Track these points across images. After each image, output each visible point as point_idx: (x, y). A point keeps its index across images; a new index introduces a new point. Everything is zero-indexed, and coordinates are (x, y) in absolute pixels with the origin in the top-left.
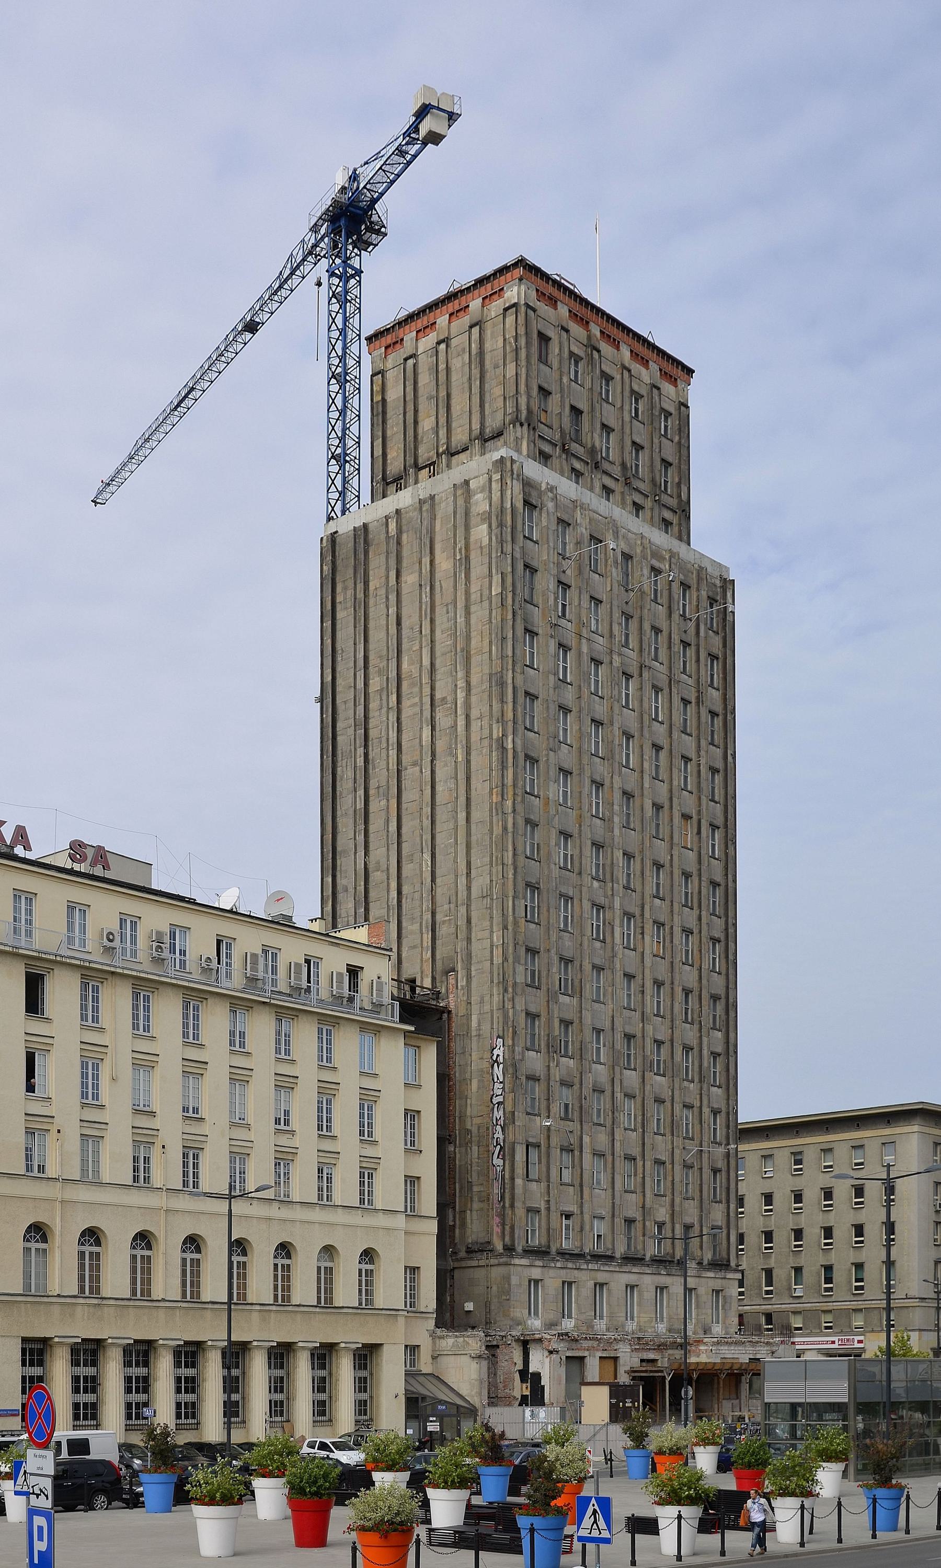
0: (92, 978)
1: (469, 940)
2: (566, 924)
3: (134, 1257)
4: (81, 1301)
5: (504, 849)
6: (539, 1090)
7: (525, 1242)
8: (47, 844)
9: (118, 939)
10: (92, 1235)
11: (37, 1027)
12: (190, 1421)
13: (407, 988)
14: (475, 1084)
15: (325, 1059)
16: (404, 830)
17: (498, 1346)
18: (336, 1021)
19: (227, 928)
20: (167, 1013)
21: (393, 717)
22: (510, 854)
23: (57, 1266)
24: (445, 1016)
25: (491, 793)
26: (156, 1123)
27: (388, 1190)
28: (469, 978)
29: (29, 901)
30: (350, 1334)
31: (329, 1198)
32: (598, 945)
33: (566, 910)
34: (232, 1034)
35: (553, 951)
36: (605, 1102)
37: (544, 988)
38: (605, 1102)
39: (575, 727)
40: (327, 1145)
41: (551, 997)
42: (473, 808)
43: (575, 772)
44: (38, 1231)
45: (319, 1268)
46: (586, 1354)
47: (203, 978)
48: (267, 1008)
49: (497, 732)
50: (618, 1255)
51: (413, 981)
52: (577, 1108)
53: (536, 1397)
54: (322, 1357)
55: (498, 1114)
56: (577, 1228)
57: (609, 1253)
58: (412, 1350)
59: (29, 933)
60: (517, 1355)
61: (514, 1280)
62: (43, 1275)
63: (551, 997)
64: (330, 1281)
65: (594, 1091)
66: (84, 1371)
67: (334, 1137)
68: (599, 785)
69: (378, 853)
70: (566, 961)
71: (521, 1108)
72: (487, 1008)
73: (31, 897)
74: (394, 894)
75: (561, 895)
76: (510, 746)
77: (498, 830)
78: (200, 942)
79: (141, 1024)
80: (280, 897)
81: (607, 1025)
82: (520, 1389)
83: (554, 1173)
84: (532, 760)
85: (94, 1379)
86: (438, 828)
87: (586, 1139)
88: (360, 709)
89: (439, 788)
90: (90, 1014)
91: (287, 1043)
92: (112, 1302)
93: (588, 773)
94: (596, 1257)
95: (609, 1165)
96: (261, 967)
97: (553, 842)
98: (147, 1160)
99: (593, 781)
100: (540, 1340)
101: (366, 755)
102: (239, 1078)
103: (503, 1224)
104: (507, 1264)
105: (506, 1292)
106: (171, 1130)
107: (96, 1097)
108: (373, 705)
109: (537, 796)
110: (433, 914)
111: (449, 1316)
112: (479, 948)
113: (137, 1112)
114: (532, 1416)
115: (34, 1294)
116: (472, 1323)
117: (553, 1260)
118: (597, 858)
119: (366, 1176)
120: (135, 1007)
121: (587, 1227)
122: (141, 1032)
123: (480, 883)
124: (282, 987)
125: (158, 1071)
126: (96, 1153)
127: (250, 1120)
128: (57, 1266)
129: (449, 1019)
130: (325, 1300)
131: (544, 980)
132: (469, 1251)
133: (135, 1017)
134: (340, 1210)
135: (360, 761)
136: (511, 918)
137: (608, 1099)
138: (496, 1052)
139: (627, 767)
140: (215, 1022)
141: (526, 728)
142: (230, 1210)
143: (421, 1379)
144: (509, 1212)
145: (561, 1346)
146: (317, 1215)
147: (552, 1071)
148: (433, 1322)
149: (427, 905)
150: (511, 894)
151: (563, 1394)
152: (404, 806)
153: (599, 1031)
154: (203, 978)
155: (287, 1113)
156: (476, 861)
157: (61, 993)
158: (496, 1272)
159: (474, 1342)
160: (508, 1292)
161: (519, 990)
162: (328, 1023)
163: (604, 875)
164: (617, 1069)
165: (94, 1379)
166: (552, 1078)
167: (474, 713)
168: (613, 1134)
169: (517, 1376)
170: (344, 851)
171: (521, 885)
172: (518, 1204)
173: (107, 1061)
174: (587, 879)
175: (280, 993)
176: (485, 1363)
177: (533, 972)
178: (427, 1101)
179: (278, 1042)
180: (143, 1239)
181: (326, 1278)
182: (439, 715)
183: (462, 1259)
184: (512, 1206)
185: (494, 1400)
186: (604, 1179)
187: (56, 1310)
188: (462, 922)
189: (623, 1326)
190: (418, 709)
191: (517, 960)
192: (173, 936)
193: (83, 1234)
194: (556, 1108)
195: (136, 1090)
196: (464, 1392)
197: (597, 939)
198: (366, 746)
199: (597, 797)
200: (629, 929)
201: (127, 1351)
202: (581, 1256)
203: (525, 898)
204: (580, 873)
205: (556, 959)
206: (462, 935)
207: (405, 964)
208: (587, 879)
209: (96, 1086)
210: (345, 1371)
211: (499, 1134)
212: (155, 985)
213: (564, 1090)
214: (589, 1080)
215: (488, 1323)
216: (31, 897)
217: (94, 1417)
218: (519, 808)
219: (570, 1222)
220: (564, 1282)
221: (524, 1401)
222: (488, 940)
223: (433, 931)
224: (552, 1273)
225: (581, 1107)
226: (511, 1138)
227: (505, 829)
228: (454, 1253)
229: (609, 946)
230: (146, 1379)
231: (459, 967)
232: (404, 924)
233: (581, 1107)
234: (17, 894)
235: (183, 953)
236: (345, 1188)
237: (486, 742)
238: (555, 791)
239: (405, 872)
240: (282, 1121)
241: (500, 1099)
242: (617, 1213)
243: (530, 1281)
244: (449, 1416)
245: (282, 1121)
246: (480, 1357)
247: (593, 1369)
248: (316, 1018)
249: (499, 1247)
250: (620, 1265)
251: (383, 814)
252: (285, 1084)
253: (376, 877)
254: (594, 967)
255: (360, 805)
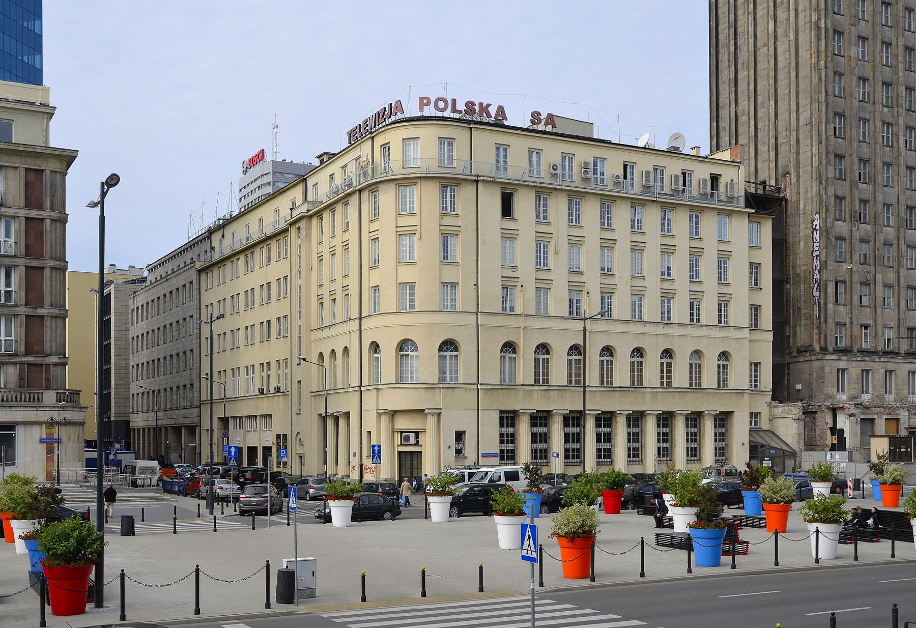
0: (542, 192)
1: (798, 153)
2: (864, 137)
3: (662, 364)
4: (536, 387)
5: (819, 92)
6: (845, 246)
7: (834, 344)
8: (518, 118)
9: (560, 169)
10: (543, 348)
11: (508, 224)
12: (607, 460)
13: (761, 187)
14: (802, 245)
15: (695, 234)
16: (759, 88)
17: (816, 412)
18: (702, 209)
19: (630, 157)
20: (590, 211)
21: (751, 18)
22: (823, 95)
23: (521, 366)
24: (783, 202)
25: (811, 58)
26: (583, 279)
27: (738, 314)
28: (798, 177)
29: (506, 150)
30: (711, 405)
31: (726, 322)
32: (887, 149)
33: (864, 128)
34: (633, 221)
35: (855, 155)
36: (893, 251)
37: (848, 180)
38: (893, 251)
39: (871, 8)
40: (696, 287)
41: (853, 185)
42: (800, 68)
43: (870, 37)
44: (510, 347)
45: (691, 365)
46: (875, 416)
47: (615, 189)
48: (655, 204)
49: (814, 18)
50: (902, 351)
51: (765, 182)
52: (872, 256)
53: (840, 445)
54: (665, 420)
55: (816, 263)
56: (873, 335)
57: (896, 351)
58: (755, 416)
59: (506, 169)
60: (829, 418)
61: (827, 369)
62: (513, 373)
63: (853, 185)
64: (698, 373)
65: (885, 244)
66: (603, 430)
67: (701, 282)
68: (888, 45)
69: (743, 104)
70: (864, 161)
71: (832, 258)
72: (809, 195)
73: (506, 147)
74: (752, 129)
75: (860, 119)
76: (823, 25)
77: (815, 81)
78: (613, 166)
79: (574, 219)
80: (677, 137)
81: (895, 201)
82: (830, 440)
83: (856, 300)
84: (839, 33)
85: (513, 435)
86: (779, 83)
87: (879, 276)
88: (732, 16)
89: (780, 59)
90: (541, 215)
91: (669, 225)
92: (556, 388)
93: (879, 38)
94: (886, 353)
95: (896, 293)
96: (652, 179)
97: (854, 85)
98: (578, 301)
99: (883, 43)
100: (843, 408)
101: (736, 44)
102: (637, 248)
103: (820, 334)
104: (822, 359)
105: (822, 377)
106: (593, 282)
107: (546, 264)
108: (740, 13)
109: (844, 56)
110: (776, 139)
111: (782, 391)
112: (804, 158)
113: (571, 272)
114: (831, 457)
115: (507, 384)
116: (801, 397)
117: (855, 356)
118: (887, 92)
119: (723, 307)
120: (570, 209)
121: (880, 334)
122: (574, 223)
123: (805, 116)
124: (667, 190)
125: (585, 247)
126: (546, 298)
127: (645, 274)
128: (521, 366)
129: (786, 204)
130: (695, 384)
131: (848, 175)
132: (799, 351)
133: (570, 215)
134: (704, 328)
135: (732, 49)
136: (824, 137)
137: (895, 250)
138: (815, 223)
139: (909, 31)
140: (622, 215)
141: (834, 13)
142: (585, 328)
143: (762, 434)
144: (823, 325)
145: (857, 412)
146: (689, 331)
147: (854, 233)
148: (770, 397)
149: (772, 133)
150: (824, 120)
151: (859, 442)
152: (758, 73)
153: (889, 206)
154: (615, 189)
155: (669, 268)
156: (802, 102)
157: (524, 204)
158: (816, 364)
159: (795, 409)
160: (823, 377)
161: (830, 182)
162: (695, 211)
163: (892, 102)
164: (902, 230)
165: (513, 435)
166: (854, 238)
167: (801, 8)
168: (899, 273)
169: (829, 431)
170: (724, 106)
171: (831, 114)
172: (830, 320)
173: (552, 243)
174: (879, 107)
175: (666, 194)
176: (802, 423)
177: (840, 170)
178: (766, 257)
179: (663, 224)
180: (638, 352)
181: (695, 371)
182: (779, 12)
183: (795, 357)
184: (826, 322)
185: (811, 445)
186: (892, 302)
187: (521, 393)
188: (793, 142)
189: (906, 398)
190: (766, 11)
191: (828, 163)
192: (595, 164)
193: (633, 351)
194: (856, 257)
195: (570, 259)
196: (789, 442)
197: (887, 145)
198: (735, 39)
199: (887, 52)
200: (910, 137)
201: (628, 418)
202: (875, 353)
203: (834, 123)
204: (874, 103)
205: (856, 161)
206: (794, 150)
207: (759, 172)
208: (879, 107)
209: (546, 258)
210: (708, 429)
211: (817, 276)
212: (582, 195)
213: (864, 245)
214: (881, 238)
215: (810, 397)
216: (506, 147)
217: (513, 458)
218: (830, 65)
219: (868, 331)
220: (863, 370)
221: (833, 448)
222: (810, 151)
223: (776, 149)
224: (854, 364)
225: (875, 256)
226: (825, 278)
227: (820, 79)
228: (790, 353)
229: (895, 150)
230: (610, 434)
231: (792, 171)
232: (759, 147)
233: (875, 256)
234: (498, 146)
235: (602, 174)
236: (708, 313)
237: (808, 26)
238: (854, 51)
239: (759, 115)
240: (666, 274)
241: (818, 253)
242: (901, 324)
243: (838, 370)
244: (779, 457)
245: (666, 274)
246: (798, 419)
247: (880, 426)
248: (659, 205)
249: (817, 348)
250: (904, 358)
251: (746, 79)
252: (668, 251)
253: (742, 119)
254: (884, 163)
255: (732, 76)
